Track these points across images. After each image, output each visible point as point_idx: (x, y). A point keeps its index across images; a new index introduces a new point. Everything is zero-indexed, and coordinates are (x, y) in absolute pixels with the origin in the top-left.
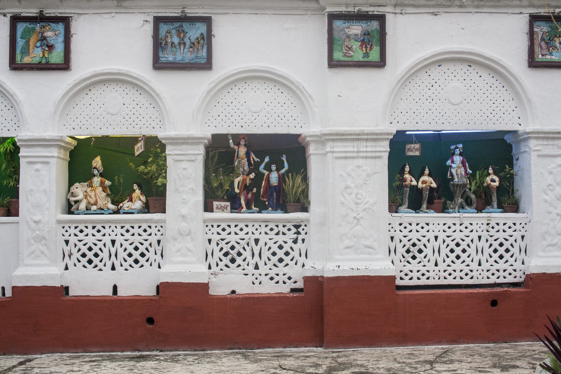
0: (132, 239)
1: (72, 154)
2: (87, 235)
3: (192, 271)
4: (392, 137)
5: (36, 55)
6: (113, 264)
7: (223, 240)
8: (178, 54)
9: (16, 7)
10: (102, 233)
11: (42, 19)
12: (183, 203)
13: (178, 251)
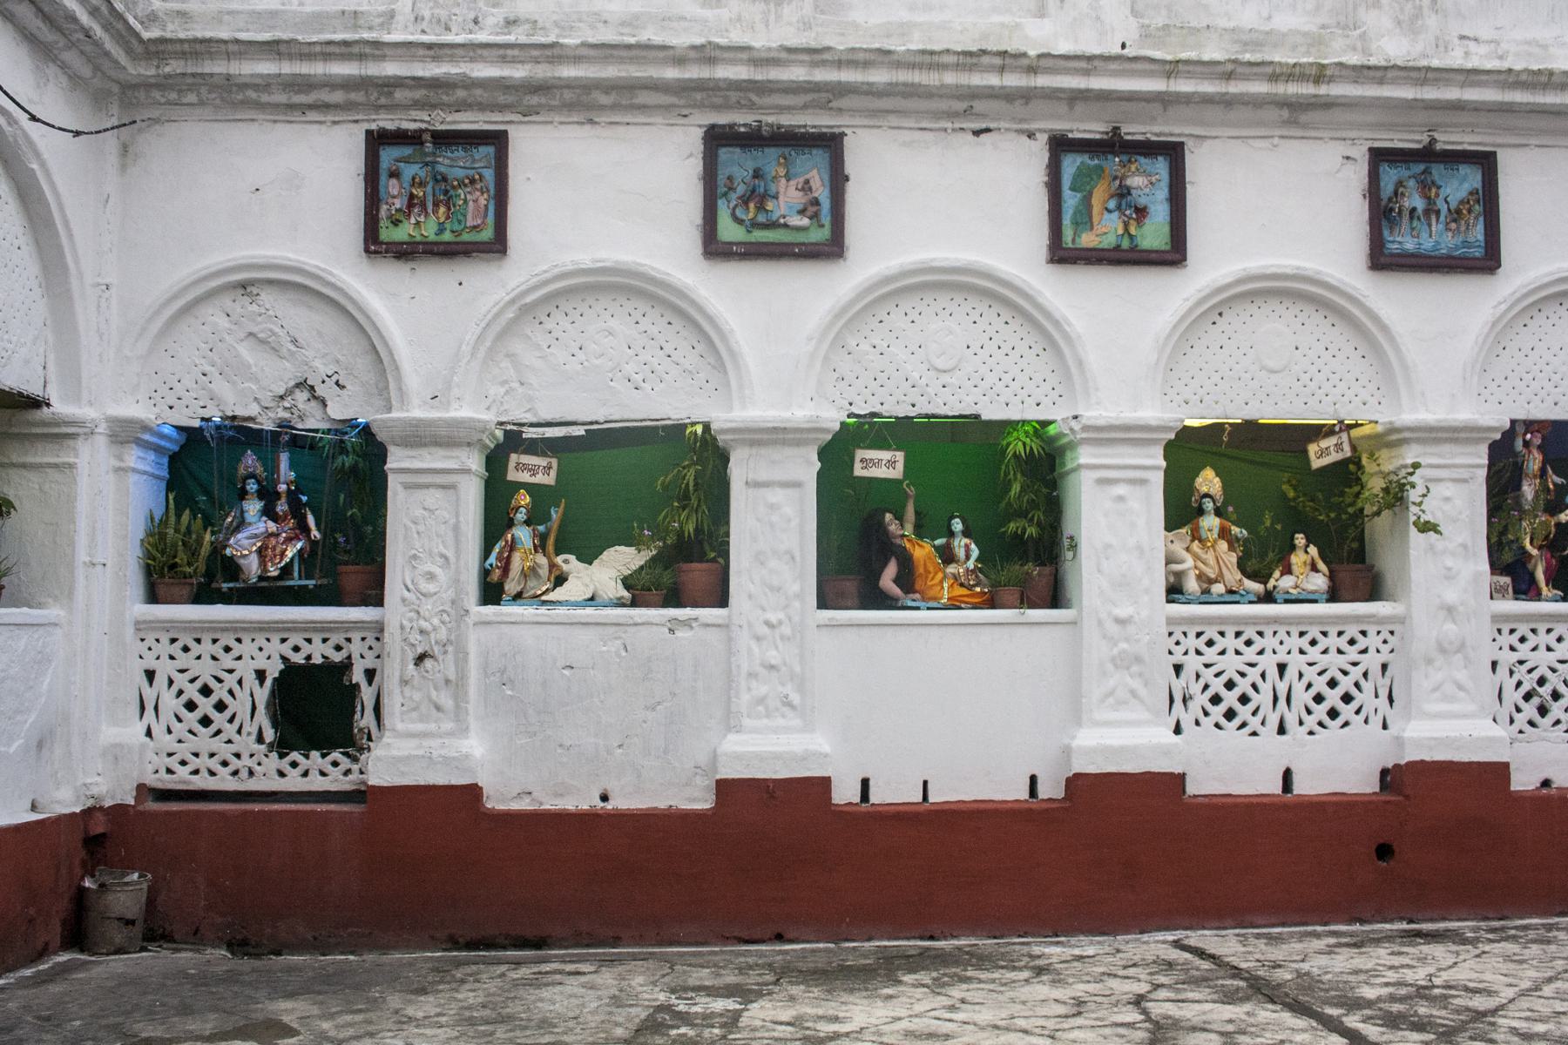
0: (1324, 661)
1: (175, 460)
2: (1223, 653)
3: (1475, 734)
4: (1172, 436)
5: (1107, 230)
6: (1178, 723)
7: (1521, 662)
8: (1424, 235)
9: (1060, 118)
10: (1255, 648)
11: (1113, 145)
12: (1447, 578)
13: (1435, 689)
